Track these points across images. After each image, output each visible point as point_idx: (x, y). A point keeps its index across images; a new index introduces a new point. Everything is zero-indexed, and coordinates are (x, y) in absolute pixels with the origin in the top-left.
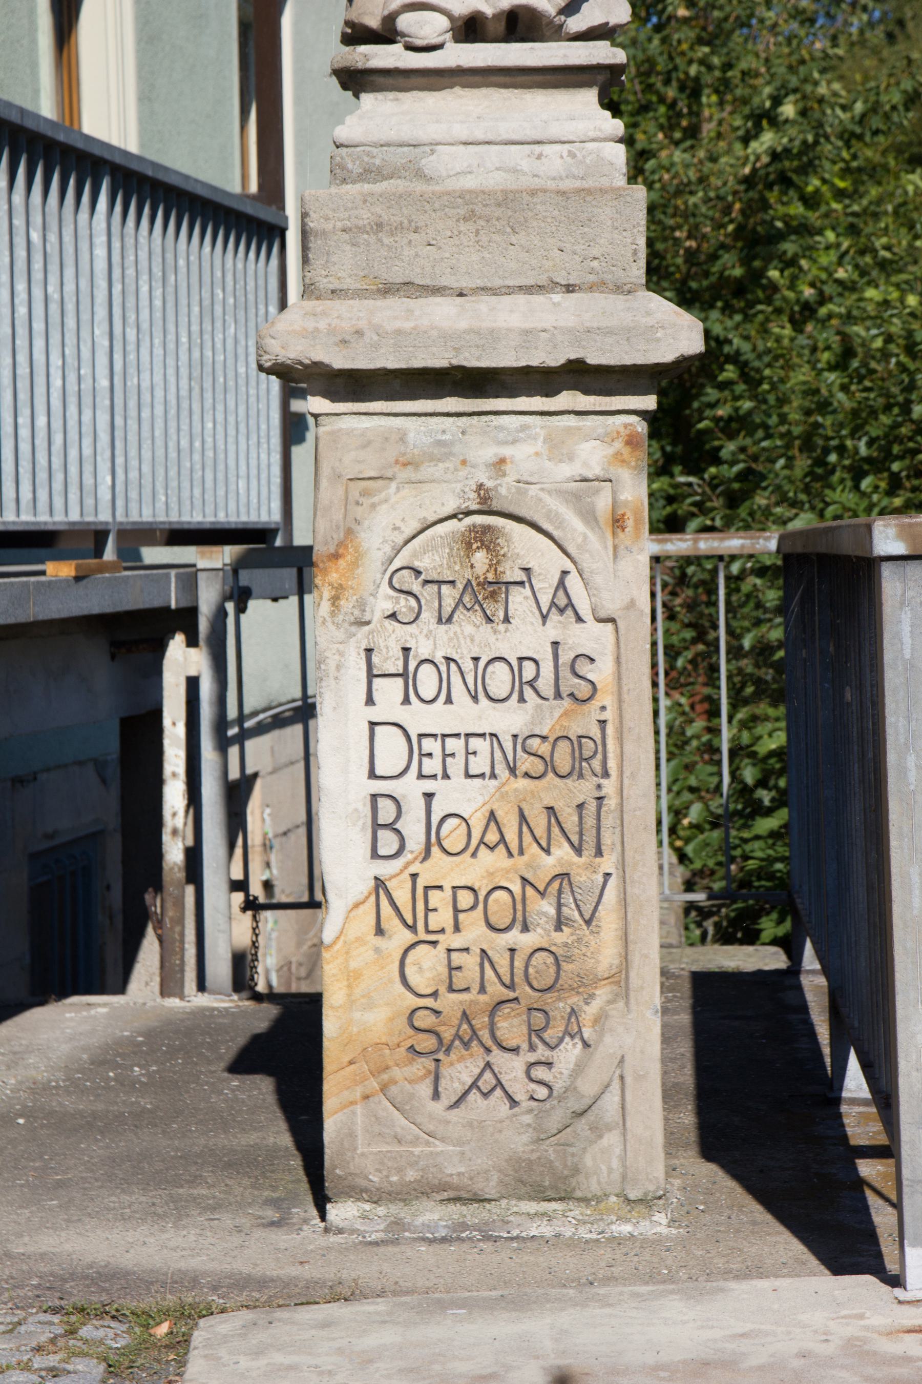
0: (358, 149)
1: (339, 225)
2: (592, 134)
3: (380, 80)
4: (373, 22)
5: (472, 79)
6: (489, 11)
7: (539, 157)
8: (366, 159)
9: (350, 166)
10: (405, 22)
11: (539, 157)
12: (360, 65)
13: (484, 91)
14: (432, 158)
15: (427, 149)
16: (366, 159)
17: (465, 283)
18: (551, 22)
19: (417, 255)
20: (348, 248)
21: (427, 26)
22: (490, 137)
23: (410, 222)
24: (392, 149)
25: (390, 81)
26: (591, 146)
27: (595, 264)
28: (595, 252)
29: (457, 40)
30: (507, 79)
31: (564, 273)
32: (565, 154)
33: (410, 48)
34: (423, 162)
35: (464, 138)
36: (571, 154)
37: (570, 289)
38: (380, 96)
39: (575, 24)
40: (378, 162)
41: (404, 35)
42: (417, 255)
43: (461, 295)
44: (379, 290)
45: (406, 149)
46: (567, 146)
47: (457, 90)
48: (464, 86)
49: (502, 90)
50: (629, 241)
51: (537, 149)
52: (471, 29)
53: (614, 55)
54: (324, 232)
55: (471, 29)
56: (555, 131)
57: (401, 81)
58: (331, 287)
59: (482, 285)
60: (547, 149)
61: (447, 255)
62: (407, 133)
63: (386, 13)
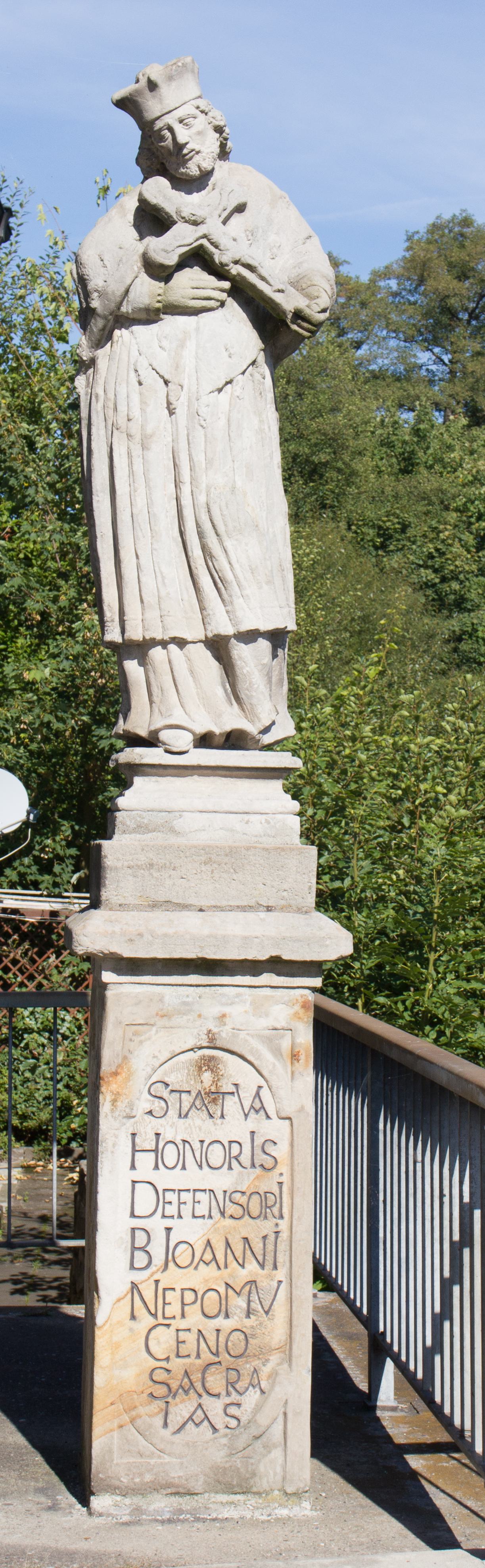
0: (134, 813)
1: (126, 864)
2: (280, 810)
3: (149, 770)
4: (143, 733)
5: (205, 772)
6: (217, 731)
7: (247, 822)
8: (139, 819)
9: (128, 823)
10: (164, 735)
11: (247, 822)
12: (137, 762)
13: (212, 778)
14: (180, 820)
15: (177, 814)
16: (139, 819)
17: (203, 903)
18: (254, 738)
19: (174, 884)
20: (131, 878)
21: (183, 740)
22: (216, 809)
23: (171, 863)
24: (155, 813)
25: (154, 770)
26: (279, 816)
27: (285, 894)
28: (285, 886)
29: (195, 747)
30: (228, 773)
31: (265, 898)
32: (263, 821)
33: (167, 751)
34: (175, 822)
35: (200, 809)
36: (268, 822)
37: (269, 909)
38: (146, 779)
39: (267, 739)
40: (146, 821)
41: (164, 744)
42: (174, 884)
43: (201, 910)
44: (149, 905)
45: (164, 814)
46: (264, 816)
47: (196, 777)
48: (199, 775)
49: (223, 779)
50: (306, 880)
51: (246, 817)
52: (204, 741)
53: (295, 763)
54: (116, 868)
55: (204, 741)
56: (257, 806)
57: (161, 771)
58: (120, 902)
59: (214, 904)
60: (252, 818)
61: (193, 885)
62: (165, 804)
63: (152, 728)
